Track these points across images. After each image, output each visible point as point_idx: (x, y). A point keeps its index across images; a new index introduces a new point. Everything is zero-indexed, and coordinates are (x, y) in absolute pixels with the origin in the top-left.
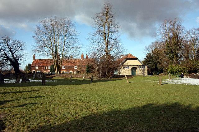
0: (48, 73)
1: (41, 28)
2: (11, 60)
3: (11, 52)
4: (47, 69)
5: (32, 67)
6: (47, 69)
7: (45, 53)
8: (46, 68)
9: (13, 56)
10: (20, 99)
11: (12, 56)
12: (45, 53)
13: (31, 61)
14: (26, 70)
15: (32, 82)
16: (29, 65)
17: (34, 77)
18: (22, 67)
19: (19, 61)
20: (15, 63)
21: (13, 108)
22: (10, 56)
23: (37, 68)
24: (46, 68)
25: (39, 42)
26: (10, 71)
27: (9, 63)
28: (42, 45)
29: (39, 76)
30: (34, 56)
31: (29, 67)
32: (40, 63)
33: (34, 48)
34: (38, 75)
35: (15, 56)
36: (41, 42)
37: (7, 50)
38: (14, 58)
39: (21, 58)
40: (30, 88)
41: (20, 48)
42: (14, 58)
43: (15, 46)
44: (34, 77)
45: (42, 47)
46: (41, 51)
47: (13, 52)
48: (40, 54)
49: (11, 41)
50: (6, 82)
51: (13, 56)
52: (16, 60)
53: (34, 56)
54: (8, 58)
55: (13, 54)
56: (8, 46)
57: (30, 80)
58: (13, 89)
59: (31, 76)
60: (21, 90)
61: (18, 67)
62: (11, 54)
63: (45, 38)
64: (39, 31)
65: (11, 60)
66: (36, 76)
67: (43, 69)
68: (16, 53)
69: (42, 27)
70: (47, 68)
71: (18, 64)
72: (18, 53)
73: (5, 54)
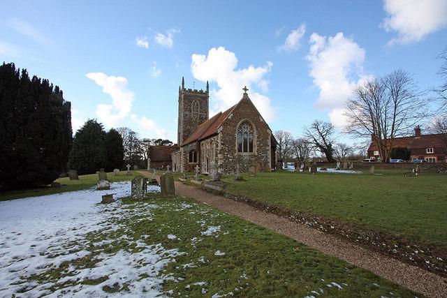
54: (318, 144)
65: (321, 147)
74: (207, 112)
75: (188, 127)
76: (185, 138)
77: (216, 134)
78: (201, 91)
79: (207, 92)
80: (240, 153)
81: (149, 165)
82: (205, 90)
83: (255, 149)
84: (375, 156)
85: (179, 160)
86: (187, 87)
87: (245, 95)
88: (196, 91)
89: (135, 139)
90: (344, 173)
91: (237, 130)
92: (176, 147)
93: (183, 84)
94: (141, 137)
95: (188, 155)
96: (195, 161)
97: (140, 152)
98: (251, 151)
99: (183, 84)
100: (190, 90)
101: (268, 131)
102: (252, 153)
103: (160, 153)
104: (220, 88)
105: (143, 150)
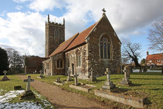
0: (161, 65)
1: (154, 30)
2: (132, 57)
3: (132, 51)
4: (160, 62)
5: (146, 61)
6: (160, 62)
7: (158, 49)
8: (158, 61)
9: (134, 54)
10: (150, 84)
11: (133, 54)
12: (158, 49)
13: (145, 57)
14: (142, 64)
15: (150, 72)
16: (144, 60)
17: (151, 68)
18: (139, 62)
19: (138, 57)
20: (135, 59)
21: (7, 89)
22: (131, 54)
23: (151, 61)
24: (158, 61)
25: (152, 41)
26: (131, 64)
27: (132, 59)
28: (156, 43)
29: (155, 68)
30: (148, 53)
31: (144, 61)
32: (154, 58)
33: (148, 47)
34: (154, 67)
35: (135, 54)
36: (154, 40)
37: (130, 51)
38: (134, 55)
39: (139, 55)
40: (146, 76)
41: (138, 48)
42: (134, 55)
43: (134, 47)
44: (151, 68)
45: (156, 44)
46: (155, 47)
47: (133, 52)
48: (153, 50)
49: (132, 45)
50: (133, 71)
51: (134, 54)
52: (136, 57)
53: (148, 53)
54: (130, 56)
55: (133, 53)
56: (130, 48)
57: (148, 71)
58: (137, 76)
59: (149, 67)
60: (147, 78)
61: (137, 61)
62: (132, 53)
63: (158, 36)
64: (152, 33)
65: (132, 57)
66: (152, 68)
67: (157, 62)
68: (135, 52)
69: (154, 29)
70: (160, 61)
71: (137, 59)
72: (137, 52)
73: (129, 54)
74: (64, 37)
75: (52, 46)
76: (50, 53)
77: (84, 43)
78: (60, 24)
79: (64, 25)
80: (102, 60)
81: (25, 70)
82: (62, 24)
83: (112, 56)
84: (150, 63)
85: (49, 70)
86: (51, 21)
87: (104, 14)
88: (57, 24)
89: (18, 55)
90: (155, 72)
91: (100, 41)
92: (45, 59)
93: (49, 18)
94: (22, 54)
95: (56, 62)
96: (61, 67)
97: (21, 64)
98: (109, 58)
99: (49, 18)
100: (53, 23)
101: (119, 43)
102: (110, 59)
103: (34, 64)
104: (102, 10)
105: (22, 62)
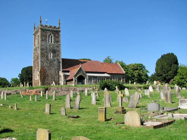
78: (55, 27)
